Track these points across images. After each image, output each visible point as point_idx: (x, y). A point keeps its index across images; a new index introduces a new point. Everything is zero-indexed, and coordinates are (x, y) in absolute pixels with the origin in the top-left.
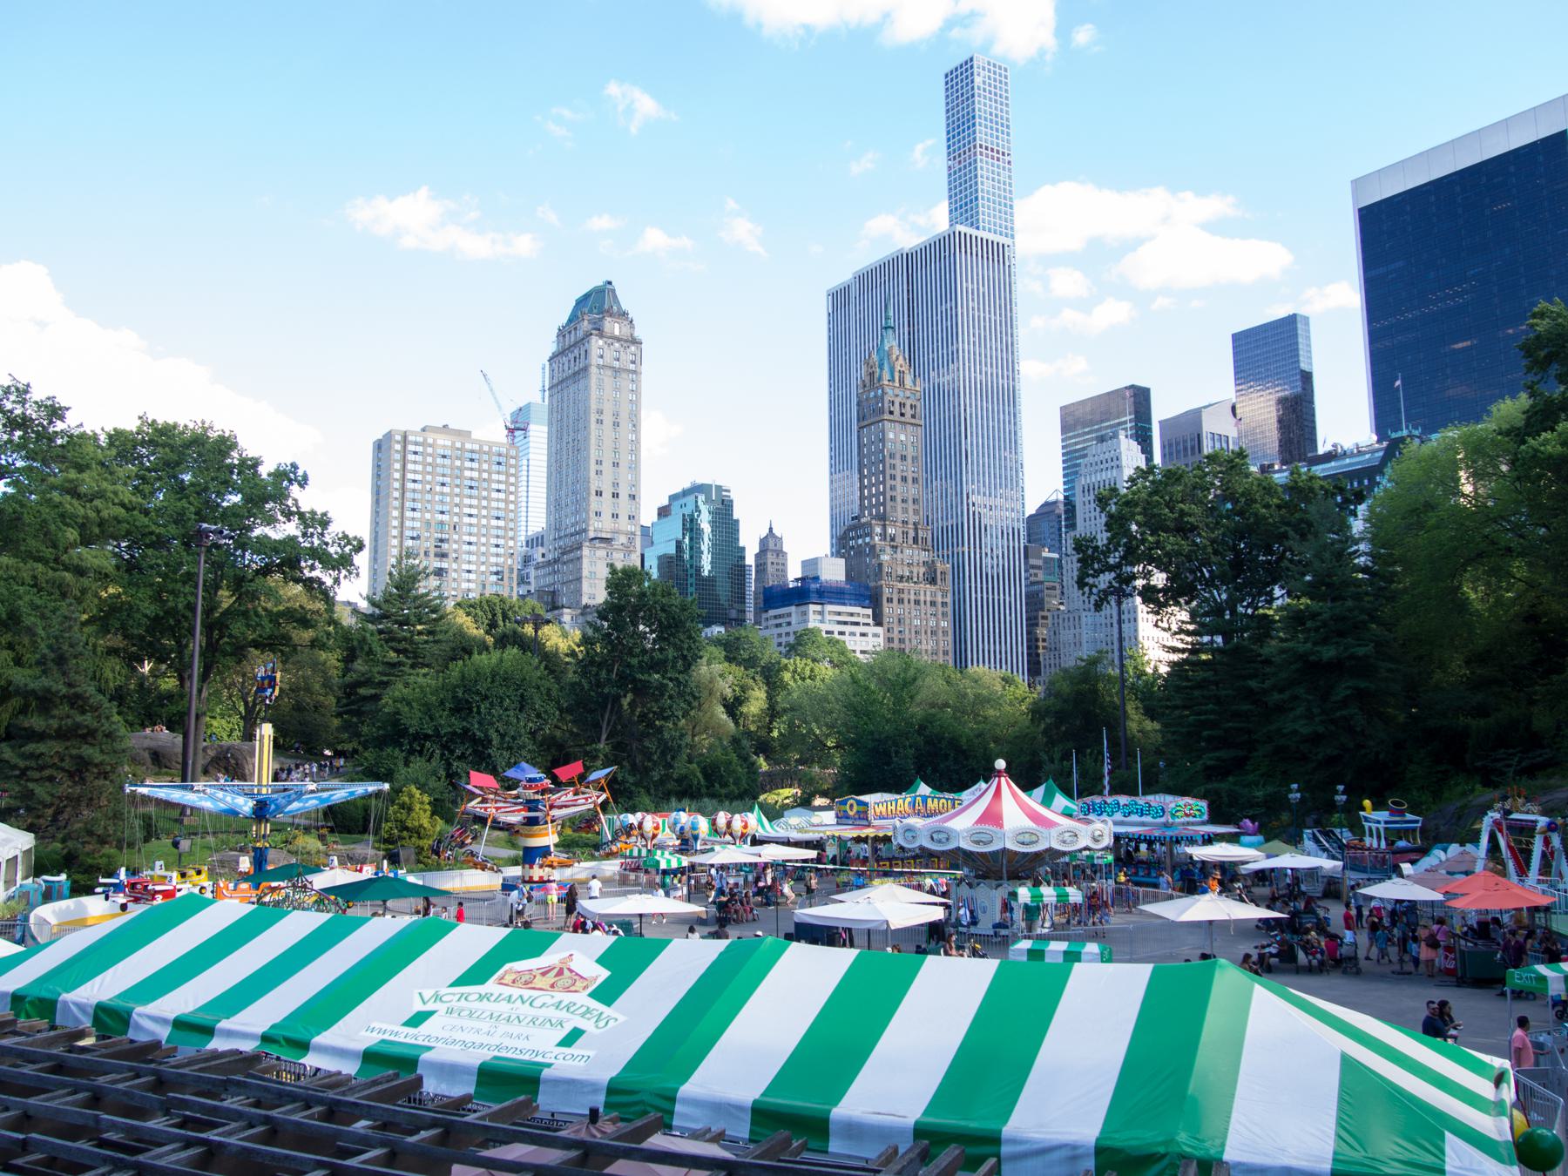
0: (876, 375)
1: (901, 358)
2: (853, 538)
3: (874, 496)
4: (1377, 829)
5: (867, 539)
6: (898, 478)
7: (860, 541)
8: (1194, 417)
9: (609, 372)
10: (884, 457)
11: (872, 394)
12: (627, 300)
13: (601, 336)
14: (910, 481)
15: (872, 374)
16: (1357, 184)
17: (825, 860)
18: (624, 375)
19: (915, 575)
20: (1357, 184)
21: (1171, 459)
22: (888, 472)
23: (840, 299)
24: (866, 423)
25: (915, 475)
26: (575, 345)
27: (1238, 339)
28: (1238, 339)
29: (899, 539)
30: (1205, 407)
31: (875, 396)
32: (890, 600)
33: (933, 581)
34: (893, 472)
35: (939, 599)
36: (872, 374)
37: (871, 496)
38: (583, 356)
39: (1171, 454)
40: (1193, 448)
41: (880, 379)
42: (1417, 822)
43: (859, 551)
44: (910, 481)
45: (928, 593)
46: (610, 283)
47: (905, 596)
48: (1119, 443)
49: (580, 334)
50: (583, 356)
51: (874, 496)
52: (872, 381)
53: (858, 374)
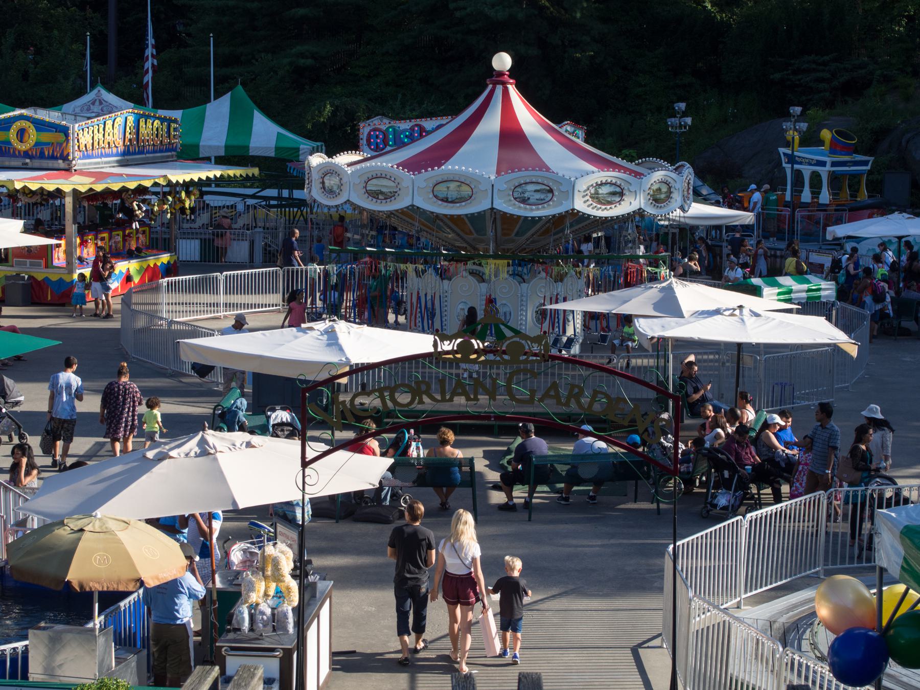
4: (815, 177)
42: (865, 163)
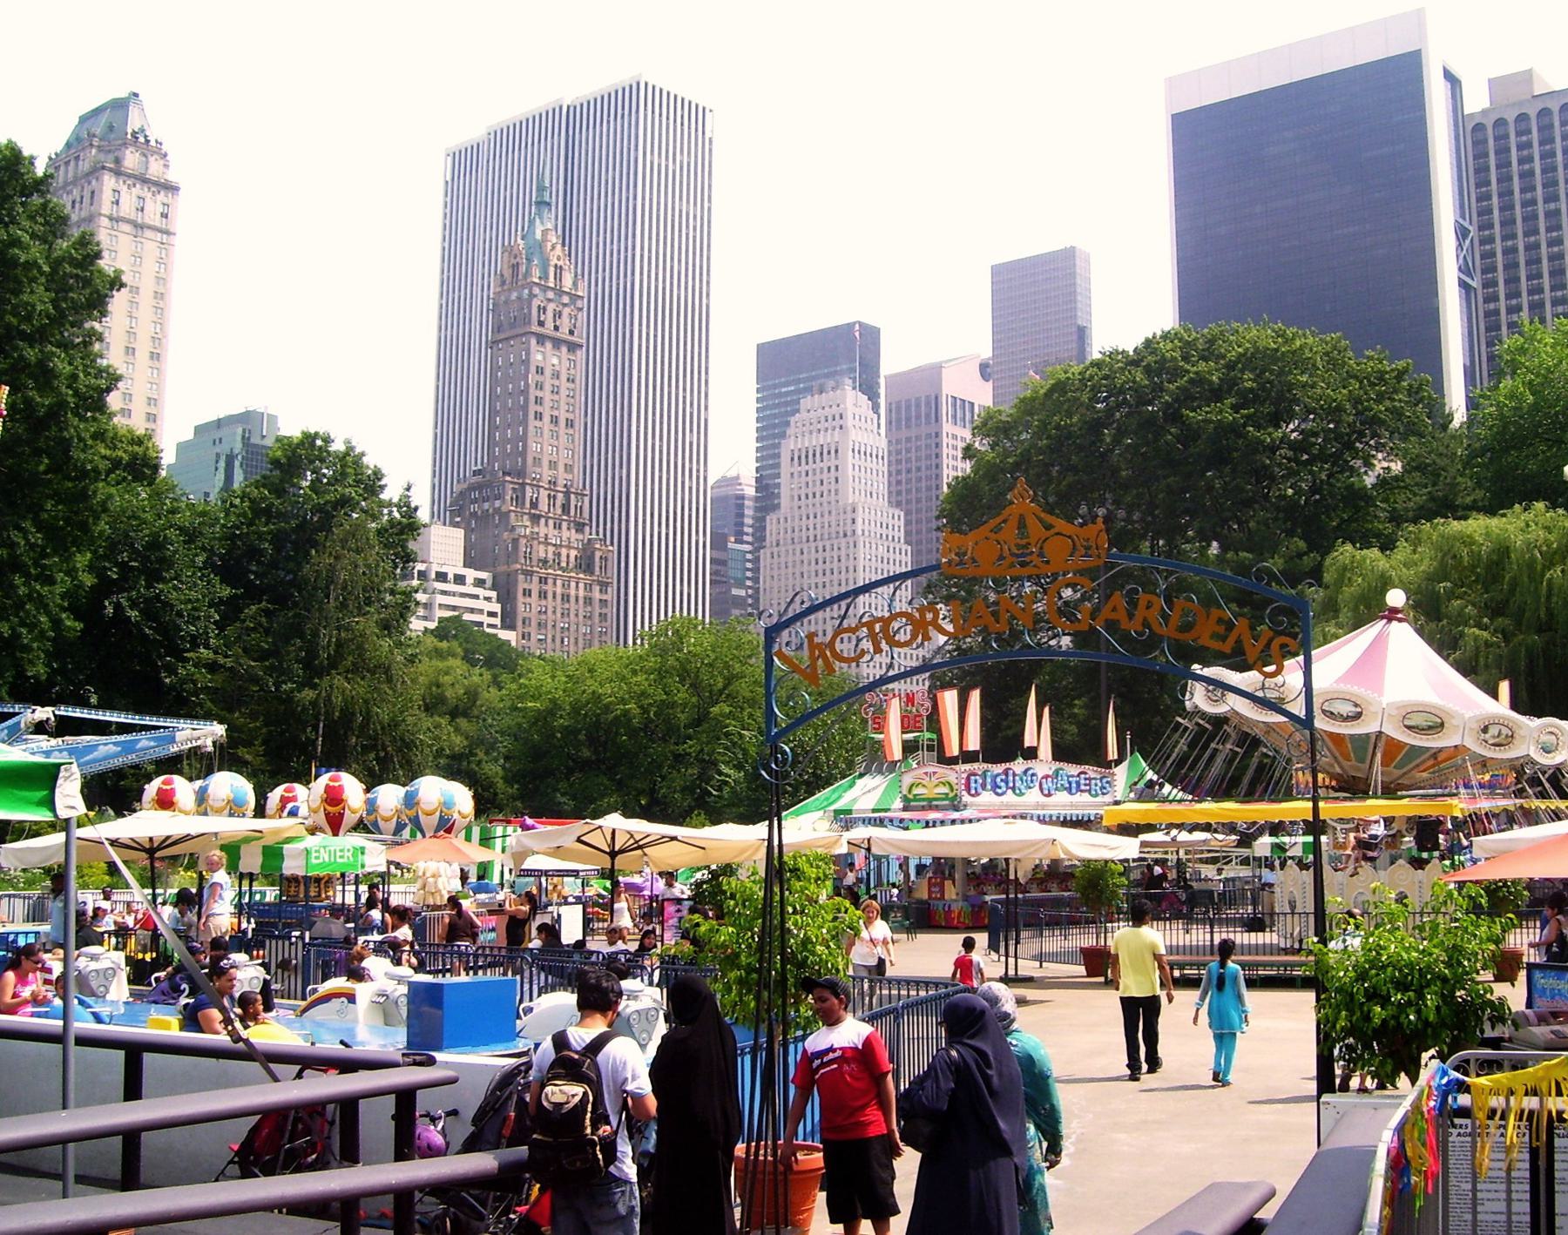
0: (523, 269)
1: (559, 247)
2: (475, 501)
3: (509, 441)
5: (497, 504)
6: (547, 419)
7: (486, 505)
8: (933, 373)
9: (127, 228)
10: (527, 385)
11: (514, 295)
12: (152, 118)
13: (118, 173)
14: (562, 423)
15: (515, 267)
16: (1171, 83)
17: (432, 1134)
18: (148, 233)
19: (564, 558)
20: (1171, 83)
21: (899, 428)
22: (532, 408)
23: (465, 162)
24: (502, 336)
25: (571, 416)
26: (75, 182)
27: (763, 350)
28: (763, 350)
29: (543, 506)
30: (946, 362)
31: (519, 298)
32: (527, 593)
33: (589, 569)
34: (539, 409)
35: (597, 595)
36: (515, 267)
37: (506, 441)
38: (86, 200)
39: (899, 421)
40: (928, 416)
41: (528, 273)
43: (483, 519)
44: (562, 423)
45: (581, 585)
46: (136, 95)
47: (549, 588)
48: (845, 397)
49: (85, 166)
50: (86, 200)
51: (509, 441)
52: (513, 276)
53: (484, 289)
